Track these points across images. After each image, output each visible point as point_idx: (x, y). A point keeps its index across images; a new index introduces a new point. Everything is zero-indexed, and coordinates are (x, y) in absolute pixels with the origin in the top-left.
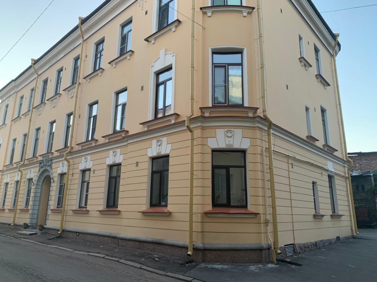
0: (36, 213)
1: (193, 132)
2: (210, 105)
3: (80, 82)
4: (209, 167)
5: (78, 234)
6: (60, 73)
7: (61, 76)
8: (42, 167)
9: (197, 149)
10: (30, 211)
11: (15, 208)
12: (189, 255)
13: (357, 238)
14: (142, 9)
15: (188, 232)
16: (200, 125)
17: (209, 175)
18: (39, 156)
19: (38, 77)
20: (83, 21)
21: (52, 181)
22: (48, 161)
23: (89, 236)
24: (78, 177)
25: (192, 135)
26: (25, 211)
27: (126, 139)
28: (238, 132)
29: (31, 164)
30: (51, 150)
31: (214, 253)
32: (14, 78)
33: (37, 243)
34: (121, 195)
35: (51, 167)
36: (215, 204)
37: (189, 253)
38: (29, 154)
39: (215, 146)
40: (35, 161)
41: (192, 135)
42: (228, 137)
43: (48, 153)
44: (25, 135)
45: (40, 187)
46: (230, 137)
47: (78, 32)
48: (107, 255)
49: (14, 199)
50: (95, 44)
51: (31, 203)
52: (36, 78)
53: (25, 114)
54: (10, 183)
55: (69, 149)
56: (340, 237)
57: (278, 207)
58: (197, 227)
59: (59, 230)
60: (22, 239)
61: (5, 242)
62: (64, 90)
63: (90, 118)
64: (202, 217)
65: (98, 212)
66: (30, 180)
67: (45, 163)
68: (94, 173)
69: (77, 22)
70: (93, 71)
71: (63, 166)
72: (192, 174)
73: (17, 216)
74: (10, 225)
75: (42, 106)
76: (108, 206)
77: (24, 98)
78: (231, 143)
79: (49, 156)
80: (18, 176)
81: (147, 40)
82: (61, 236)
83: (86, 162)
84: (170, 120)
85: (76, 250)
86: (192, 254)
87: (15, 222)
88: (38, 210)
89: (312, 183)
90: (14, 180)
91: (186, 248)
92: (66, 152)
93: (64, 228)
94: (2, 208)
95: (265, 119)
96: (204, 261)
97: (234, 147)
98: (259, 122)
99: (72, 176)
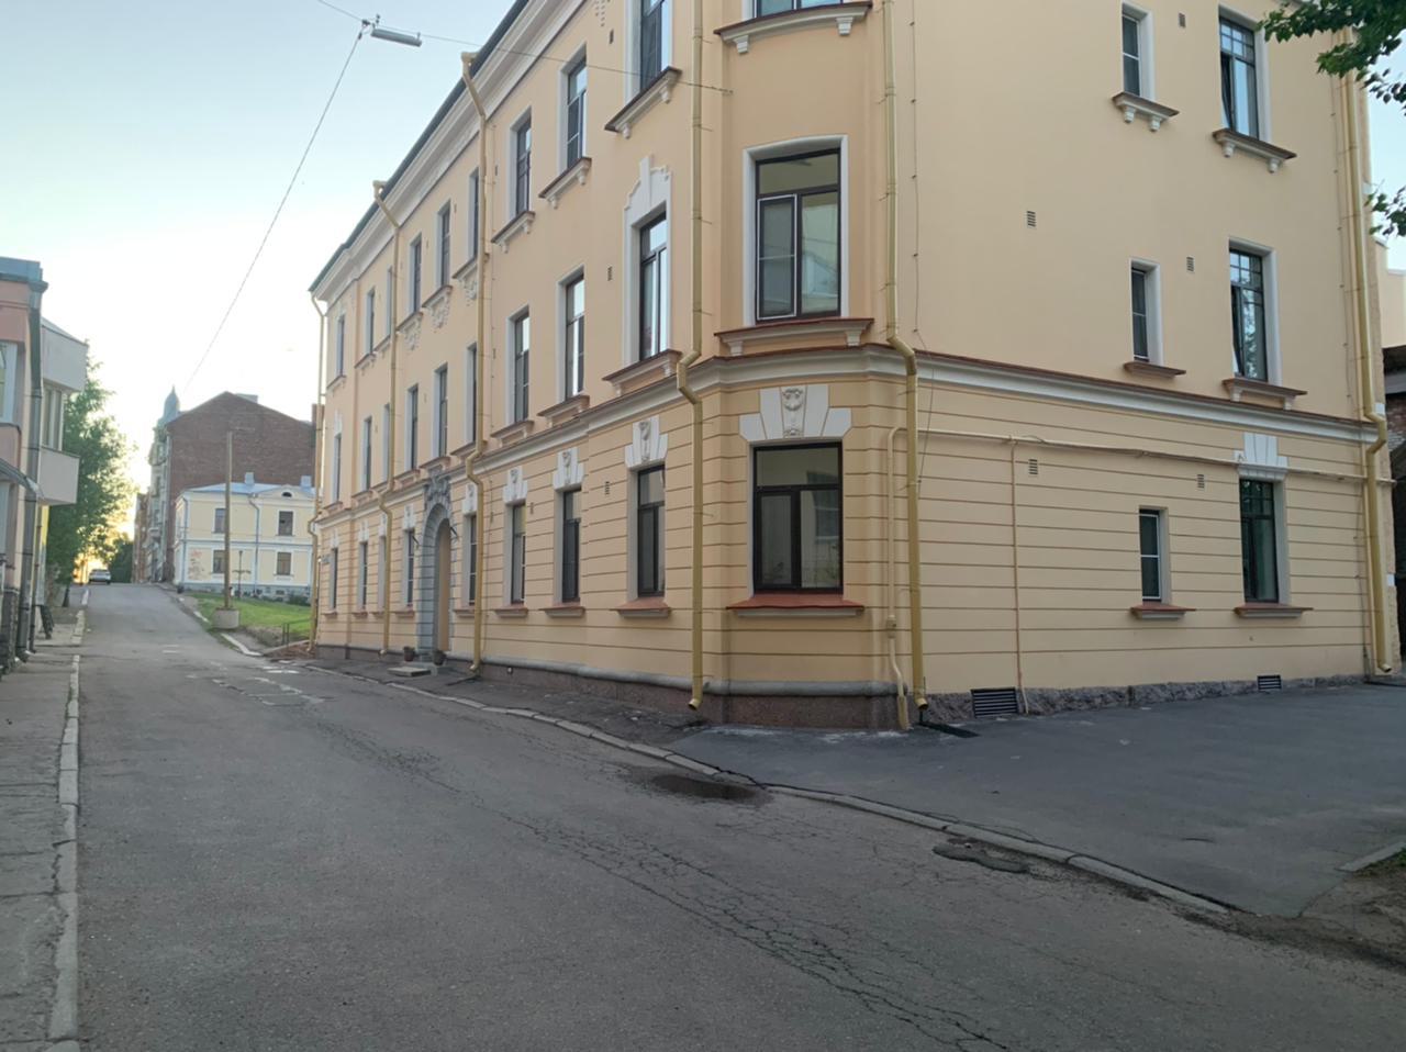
0: (431, 621)
1: (701, 403)
2: (748, 321)
3: (487, 251)
4: (745, 492)
5: (510, 670)
6: (525, 136)
7: (528, 145)
8: (430, 498)
9: (710, 449)
10: (417, 615)
11: (475, 607)
12: (691, 706)
13: (1397, 683)
14: (602, 25)
15: (691, 654)
16: (717, 381)
17: (745, 512)
18: (541, 414)
19: (398, 235)
20: (475, 64)
21: (453, 535)
22: (441, 482)
23: (530, 673)
24: (502, 521)
25: (699, 412)
26: (406, 615)
27: (582, 421)
28: (818, 395)
29: (634, 396)
30: (526, 414)
31: (753, 702)
32: (344, 239)
33: (420, 692)
34: (582, 571)
35: (449, 498)
36: (761, 586)
37: (692, 702)
38: (402, 466)
39: (758, 437)
40: (525, 435)
41: (699, 412)
42: (788, 408)
43: (516, 424)
44: (473, 350)
45: (432, 551)
46: (796, 409)
47: (467, 100)
48: (542, 714)
49: (469, 579)
50: (513, 129)
51: (416, 595)
52: (480, 135)
53: (466, 273)
54: (489, 514)
55: (476, 448)
56: (1282, 678)
57: (1176, 574)
58: (711, 642)
59: (471, 662)
60: (393, 685)
61: (353, 691)
62: (542, 196)
63: (569, 324)
64: (726, 619)
65: (542, 612)
66: (411, 532)
67: (435, 488)
68: (532, 512)
69: (457, 72)
70: (514, 216)
71: (568, 466)
72: (699, 515)
73: (392, 629)
74: (378, 652)
75: (414, 323)
76: (565, 599)
77: (376, 295)
78: (799, 425)
79: (441, 466)
80: (471, 495)
81: (610, 127)
82: (479, 676)
83: (646, 438)
84: (661, 369)
85: (489, 705)
86: (700, 706)
87: (390, 644)
88: (435, 612)
89: (1137, 511)
90: (551, 485)
91: (688, 691)
92: (470, 458)
93: (483, 656)
94: (407, 610)
95: (891, 347)
96: (727, 721)
97: (806, 436)
98: (875, 359)
99: (492, 521)
